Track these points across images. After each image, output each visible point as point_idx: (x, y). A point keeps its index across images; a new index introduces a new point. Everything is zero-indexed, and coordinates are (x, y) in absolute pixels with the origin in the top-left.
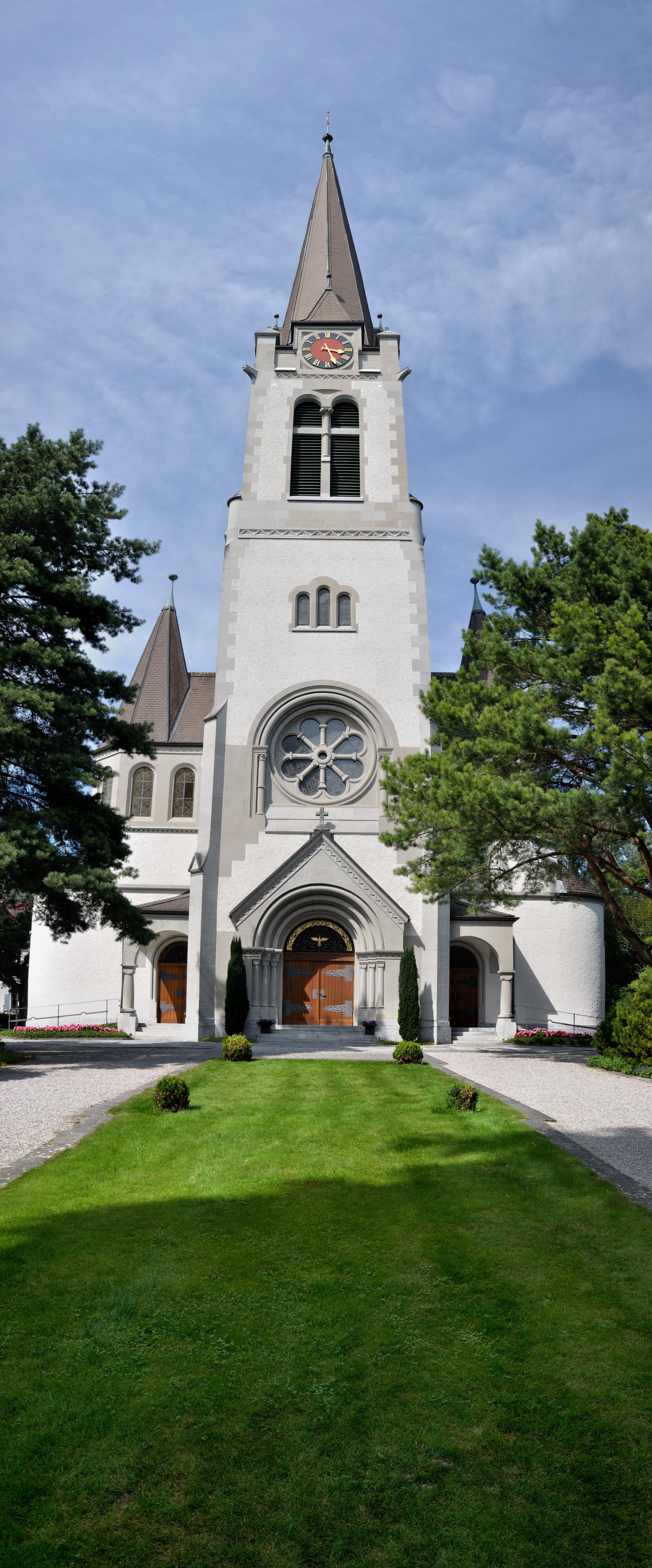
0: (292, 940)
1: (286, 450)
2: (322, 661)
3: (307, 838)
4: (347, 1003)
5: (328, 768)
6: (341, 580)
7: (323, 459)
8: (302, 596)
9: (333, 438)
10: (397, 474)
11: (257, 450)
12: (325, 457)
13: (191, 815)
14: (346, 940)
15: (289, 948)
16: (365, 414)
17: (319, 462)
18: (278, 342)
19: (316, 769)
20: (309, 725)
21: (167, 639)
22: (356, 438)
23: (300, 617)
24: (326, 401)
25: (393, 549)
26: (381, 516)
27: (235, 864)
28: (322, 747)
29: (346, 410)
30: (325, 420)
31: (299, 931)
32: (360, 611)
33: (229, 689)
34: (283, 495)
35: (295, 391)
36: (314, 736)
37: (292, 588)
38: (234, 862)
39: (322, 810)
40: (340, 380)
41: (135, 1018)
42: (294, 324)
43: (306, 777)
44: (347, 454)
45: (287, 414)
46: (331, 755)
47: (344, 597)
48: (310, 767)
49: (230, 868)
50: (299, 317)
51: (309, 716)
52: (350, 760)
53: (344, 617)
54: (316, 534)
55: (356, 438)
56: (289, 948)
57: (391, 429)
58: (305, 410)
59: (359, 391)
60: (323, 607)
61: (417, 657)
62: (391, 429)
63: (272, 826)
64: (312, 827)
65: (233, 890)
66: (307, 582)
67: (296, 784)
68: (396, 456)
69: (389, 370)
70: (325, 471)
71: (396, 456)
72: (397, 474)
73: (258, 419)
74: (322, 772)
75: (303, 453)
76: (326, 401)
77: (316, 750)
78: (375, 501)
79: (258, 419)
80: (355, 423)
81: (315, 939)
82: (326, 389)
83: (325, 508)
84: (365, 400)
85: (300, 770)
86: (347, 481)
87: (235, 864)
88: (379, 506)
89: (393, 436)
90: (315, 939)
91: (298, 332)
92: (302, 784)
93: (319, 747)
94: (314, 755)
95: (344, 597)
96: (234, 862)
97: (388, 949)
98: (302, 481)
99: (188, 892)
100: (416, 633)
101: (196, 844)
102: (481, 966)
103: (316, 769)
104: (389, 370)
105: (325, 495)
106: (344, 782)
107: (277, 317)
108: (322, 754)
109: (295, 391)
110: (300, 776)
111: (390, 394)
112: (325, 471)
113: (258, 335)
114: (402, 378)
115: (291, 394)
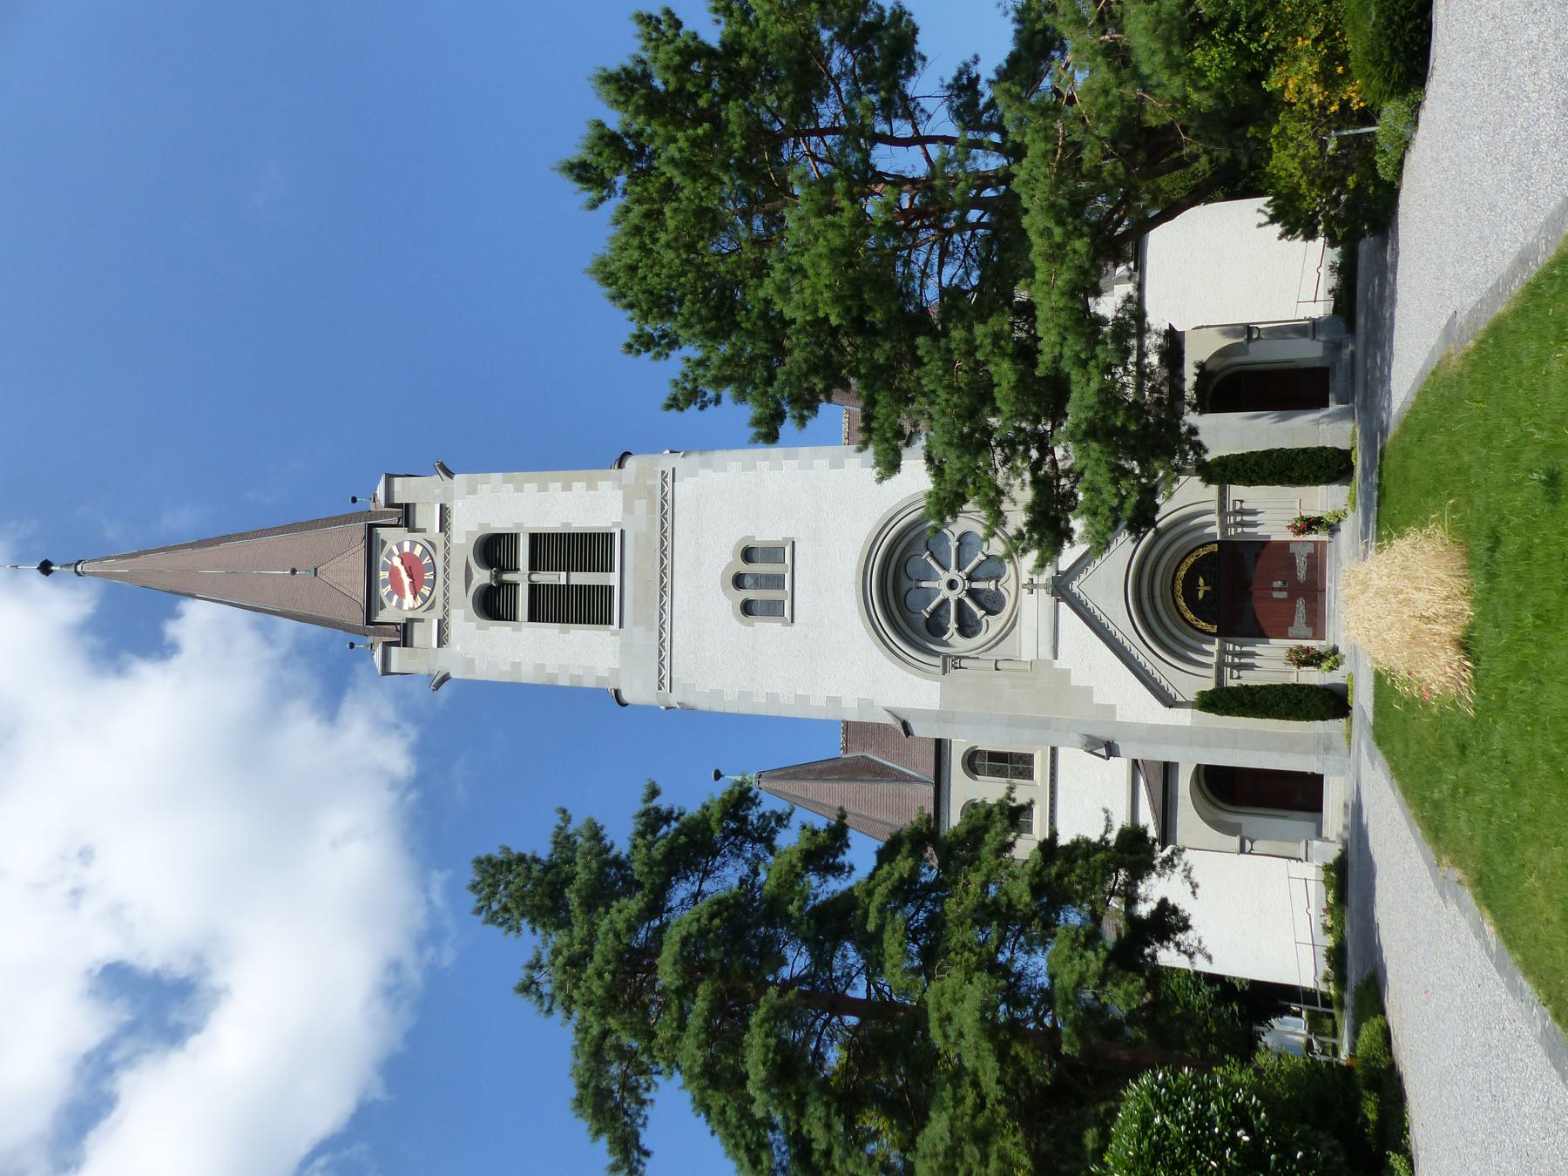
0: (1202, 624)
1: (549, 632)
2: (832, 584)
3: (1063, 605)
4: (1293, 549)
5: (970, 578)
6: (725, 558)
7: (563, 582)
8: (747, 608)
9: (533, 567)
10: (584, 484)
11: (551, 669)
12: (561, 578)
13: (1031, 756)
14: (1202, 552)
15: (1214, 629)
16: (500, 525)
17: (568, 587)
18: (396, 644)
19: (972, 593)
20: (912, 599)
21: (797, 783)
22: (534, 538)
23: (773, 610)
24: (482, 577)
25: (684, 489)
26: (641, 506)
27: (1098, 699)
28: (945, 577)
29: (494, 549)
30: (507, 577)
31: (1189, 616)
32: (766, 534)
33: (865, 704)
34: (613, 633)
35: (467, 619)
36: (929, 595)
37: (736, 623)
38: (1095, 701)
39: (1024, 586)
40: (451, 557)
41: (1192, 697)
42: (369, 621)
43: (981, 606)
44: (553, 548)
45: (499, 631)
46: (953, 573)
47: (748, 554)
48: (968, 601)
49: (1104, 706)
50: (358, 619)
51: (902, 602)
52: (958, 550)
53: (773, 553)
54: (665, 588)
55: (534, 538)
56: (1214, 629)
57: (546, 490)
58: (493, 605)
59: (468, 533)
60: (760, 582)
61: (826, 462)
62: (546, 490)
63: (1046, 652)
64: (1046, 599)
65: (1130, 703)
66: (726, 603)
67: (991, 618)
68: (559, 485)
69: (437, 491)
70: (580, 578)
71: (559, 485)
72: (584, 484)
73: (508, 668)
74: (975, 585)
75: (553, 607)
76: (482, 577)
77: (945, 593)
78: (620, 514)
79: (508, 668)
80: (514, 538)
81: (1201, 595)
82: (463, 577)
83: (628, 578)
84: (481, 525)
85: (973, 615)
86: (590, 549)
87: (1098, 699)
88: (628, 508)
89: (530, 488)
90: (1201, 595)
91: (382, 617)
92: (990, 612)
93: (942, 585)
94: (953, 596)
95: (748, 554)
96: (1095, 701)
97: (1214, 506)
98: (590, 608)
99: (1135, 762)
100: (794, 463)
101: (1074, 761)
102: (1232, 370)
103: (960, 602)
104: (437, 491)
105: (613, 579)
106: (988, 557)
107: (352, 645)
108: (952, 585)
109: (467, 619)
110: (980, 613)
111: (472, 491)
112: (580, 578)
113: (386, 671)
114: (450, 474)
115: (473, 624)
